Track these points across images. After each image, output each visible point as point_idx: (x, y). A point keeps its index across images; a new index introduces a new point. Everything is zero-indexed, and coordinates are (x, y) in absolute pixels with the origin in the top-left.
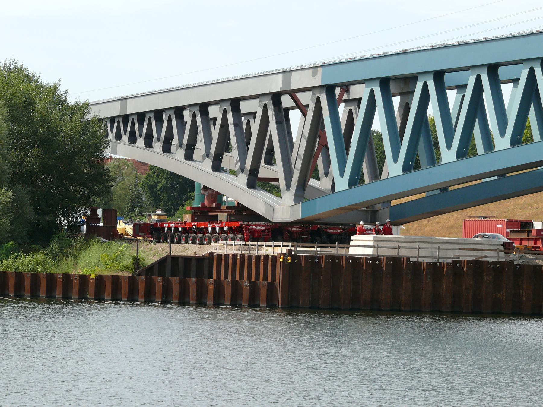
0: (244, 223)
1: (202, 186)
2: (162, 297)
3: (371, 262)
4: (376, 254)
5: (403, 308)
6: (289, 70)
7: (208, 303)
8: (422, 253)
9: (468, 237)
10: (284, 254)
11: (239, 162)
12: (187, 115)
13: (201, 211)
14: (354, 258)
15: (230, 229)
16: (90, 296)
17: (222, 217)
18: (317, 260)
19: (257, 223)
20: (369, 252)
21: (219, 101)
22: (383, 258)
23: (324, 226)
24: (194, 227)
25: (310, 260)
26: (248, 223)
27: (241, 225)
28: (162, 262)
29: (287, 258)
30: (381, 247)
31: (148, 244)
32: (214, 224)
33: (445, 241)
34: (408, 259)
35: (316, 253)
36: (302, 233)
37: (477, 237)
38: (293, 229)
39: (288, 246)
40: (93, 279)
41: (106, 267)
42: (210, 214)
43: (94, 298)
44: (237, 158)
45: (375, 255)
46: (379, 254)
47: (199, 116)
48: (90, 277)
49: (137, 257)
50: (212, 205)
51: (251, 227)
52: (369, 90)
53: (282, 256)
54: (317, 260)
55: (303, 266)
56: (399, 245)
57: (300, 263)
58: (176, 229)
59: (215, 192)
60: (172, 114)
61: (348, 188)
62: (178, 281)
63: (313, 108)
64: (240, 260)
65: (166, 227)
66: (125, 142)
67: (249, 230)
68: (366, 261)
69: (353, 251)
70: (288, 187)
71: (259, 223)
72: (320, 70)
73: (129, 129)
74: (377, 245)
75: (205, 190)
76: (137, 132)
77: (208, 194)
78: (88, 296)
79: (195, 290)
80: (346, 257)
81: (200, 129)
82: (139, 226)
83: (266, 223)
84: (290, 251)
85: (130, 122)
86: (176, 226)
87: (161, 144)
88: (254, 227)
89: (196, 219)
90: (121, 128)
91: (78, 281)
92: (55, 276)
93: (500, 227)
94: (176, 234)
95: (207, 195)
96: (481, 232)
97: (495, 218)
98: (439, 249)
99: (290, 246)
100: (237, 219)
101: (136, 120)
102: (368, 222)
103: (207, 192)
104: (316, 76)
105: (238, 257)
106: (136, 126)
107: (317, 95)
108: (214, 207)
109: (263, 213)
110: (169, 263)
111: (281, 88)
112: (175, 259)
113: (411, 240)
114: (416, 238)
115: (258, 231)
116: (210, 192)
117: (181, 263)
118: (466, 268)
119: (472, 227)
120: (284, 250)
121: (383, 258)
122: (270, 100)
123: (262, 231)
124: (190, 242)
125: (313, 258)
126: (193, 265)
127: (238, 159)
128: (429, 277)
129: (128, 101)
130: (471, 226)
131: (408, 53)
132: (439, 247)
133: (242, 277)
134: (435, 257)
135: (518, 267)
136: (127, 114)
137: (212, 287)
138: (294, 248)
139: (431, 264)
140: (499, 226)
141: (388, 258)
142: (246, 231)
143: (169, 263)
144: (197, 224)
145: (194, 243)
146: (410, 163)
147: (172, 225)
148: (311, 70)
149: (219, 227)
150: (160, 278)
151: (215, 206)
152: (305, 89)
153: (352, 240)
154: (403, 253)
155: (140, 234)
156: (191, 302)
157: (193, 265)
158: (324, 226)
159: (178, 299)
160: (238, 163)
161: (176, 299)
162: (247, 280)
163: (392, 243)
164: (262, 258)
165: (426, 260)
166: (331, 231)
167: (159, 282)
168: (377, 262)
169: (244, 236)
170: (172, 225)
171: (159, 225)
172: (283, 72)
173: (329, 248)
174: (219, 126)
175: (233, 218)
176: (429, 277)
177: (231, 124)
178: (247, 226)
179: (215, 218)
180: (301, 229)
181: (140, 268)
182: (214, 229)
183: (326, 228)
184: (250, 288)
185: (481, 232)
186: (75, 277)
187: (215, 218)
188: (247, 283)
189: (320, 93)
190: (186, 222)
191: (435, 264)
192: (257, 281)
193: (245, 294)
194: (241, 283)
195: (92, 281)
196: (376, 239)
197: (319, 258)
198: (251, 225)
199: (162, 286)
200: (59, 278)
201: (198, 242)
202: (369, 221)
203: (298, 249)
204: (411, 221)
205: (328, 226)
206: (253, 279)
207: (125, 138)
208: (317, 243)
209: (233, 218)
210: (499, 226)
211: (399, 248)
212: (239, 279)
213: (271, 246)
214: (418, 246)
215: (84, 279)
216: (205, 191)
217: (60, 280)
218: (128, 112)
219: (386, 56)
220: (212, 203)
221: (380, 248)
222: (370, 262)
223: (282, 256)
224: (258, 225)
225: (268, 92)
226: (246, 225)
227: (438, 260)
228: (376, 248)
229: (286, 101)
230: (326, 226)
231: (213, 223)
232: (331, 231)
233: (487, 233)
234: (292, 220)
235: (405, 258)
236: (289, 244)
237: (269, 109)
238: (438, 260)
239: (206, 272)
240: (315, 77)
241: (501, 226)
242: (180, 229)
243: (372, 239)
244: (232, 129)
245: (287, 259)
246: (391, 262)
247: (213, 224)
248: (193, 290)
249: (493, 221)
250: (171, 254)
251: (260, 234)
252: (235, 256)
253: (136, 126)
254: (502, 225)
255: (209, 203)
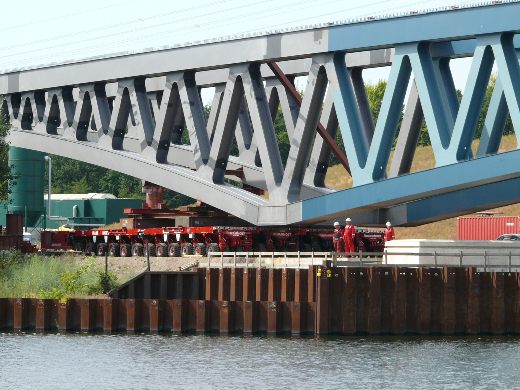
0: (219, 228)
1: (143, 183)
2: (159, 325)
3: (429, 274)
4: (434, 264)
5: (469, 331)
6: (278, 32)
7: (221, 331)
8: (494, 261)
9: (469, 238)
10: (322, 267)
11: (200, 151)
12: (76, 93)
13: (143, 215)
14: (389, 268)
15: (198, 237)
16: (60, 326)
17: (182, 221)
18: (361, 273)
19: (235, 228)
20: (414, 261)
21: (164, 73)
22: (444, 269)
23: (315, 230)
24: (140, 234)
25: (354, 274)
26: (224, 228)
27: (216, 231)
28: (139, 280)
29: (326, 272)
30: (440, 255)
31: (84, 258)
32: (173, 230)
33: (503, 245)
34: (474, 269)
35: (361, 264)
36: (289, 239)
37: (502, 238)
38: (278, 234)
39: (323, 256)
40: (64, 304)
41: (68, 288)
42: (156, 218)
43: (203, 330)
44: (196, 146)
45: (433, 265)
46: (438, 264)
47: (134, 93)
48: (60, 302)
49: (107, 275)
50: (157, 207)
51: (228, 233)
52: (401, 57)
53: (320, 270)
54: (361, 273)
55: (346, 281)
56: (461, 252)
57: (341, 276)
58: (112, 238)
59: (160, 190)
60: (91, 91)
61: (372, 181)
62: (180, 304)
63: (314, 80)
64: (249, 276)
65: (95, 235)
66: (16, 128)
67: (225, 236)
68: (399, 273)
69: (392, 261)
70: (279, 179)
71: (238, 228)
72: (326, 33)
73: (21, 111)
74: (435, 252)
75: (148, 187)
76: (35, 114)
77: (151, 192)
78: (58, 326)
79: (203, 315)
80: (423, 269)
81: (136, 109)
82: (50, 235)
83: (246, 228)
84: (328, 263)
85: (23, 103)
86: (111, 234)
87: (74, 130)
88: (231, 233)
89: (139, 224)
90: (9, 110)
91: (43, 308)
92: (11, 301)
93: (511, 226)
94: (101, 244)
95: (150, 193)
96: (506, 232)
97: (502, 215)
98: (510, 255)
99: (326, 256)
100: (202, 223)
101: (32, 99)
102: (376, 224)
103: (151, 190)
104: (320, 40)
105: (245, 272)
106: (34, 107)
107: (321, 65)
108: (161, 208)
109: (242, 215)
110: (148, 281)
111: (264, 56)
112: (156, 277)
113: (464, 245)
114: (469, 243)
115: (236, 238)
116: (155, 190)
117: (163, 282)
118: (396, 277)
119: (470, 226)
120: (319, 262)
121: (444, 269)
122: (246, 72)
123: (242, 238)
124: (135, 254)
125: (358, 270)
126: (179, 283)
127: (198, 147)
128: (500, 291)
129: (21, 75)
130: (469, 226)
131: (463, 10)
132: (510, 252)
133: (264, 296)
134: (506, 266)
135: (510, 274)
136: (20, 91)
137: (226, 311)
138: (334, 259)
139: (503, 274)
140: (509, 224)
141: (451, 269)
142: (222, 238)
143: (148, 281)
144: (146, 231)
145: (165, 254)
146: (465, 148)
147: (105, 233)
148: (312, 33)
149: (180, 234)
150: (155, 301)
151: (161, 208)
152: (303, 56)
153: (387, 247)
154: (468, 261)
155: (53, 245)
156: (198, 330)
157: (179, 283)
158: (315, 230)
159: (111, 326)
160: (198, 151)
161: (177, 326)
162: (274, 300)
163: (442, 249)
164: (233, 272)
165: (499, 270)
166: (324, 235)
167: (154, 305)
168: (436, 274)
169: (219, 245)
170: (105, 233)
171: (83, 234)
172: (268, 36)
173: (369, 257)
174: (167, 106)
175: (197, 222)
176: (500, 291)
177: (185, 103)
178: (223, 232)
179: (171, 223)
180: (288, 235)
181: (111, 289)
182: (172, 237)
183: (317, 233)
184: (277, 311)
185: (506, 232)
186: (39, 303)
187: (171, 223)
188: (273, 305)
189: (326, 62)
190: (125, 229)
191: (506, 274)
192: (214, 301)
193: (271, 319)
194: (264, 305)
195: (62, 307)
196: (423, 245)
197: (364, 270)
198: (227, 230)
199: (275, 314)
200: (271, 308)
201: (123, 254)
202: (378, 222)
203: (338, 259)
204: (432, 221)
205: (319, 230)
206: (233, 298)
207: (16, 123)
208: (360, 251)
209: (197, 222)
210: (509, 224)
211: (461, 255)
212: (287, 300)
213: (270, 256)
214: (486, 252)
215: (28, 303)
216: (148, 188)
217: (19, 306)
218: (21, 90)
219: (428, 14)
220: (157, 204)
221: (439, 256)
222: (353, 273)
223: (320, 270)
224: (236, 231)
225: (245, 61)
226: (223, 230)
227: (510, 270)
228: (434, 256)
229: (265, 71)
230: (317, 230)
231: (171, 229)
232: (324, 235)
233: (517, 233)
234: (289, 223)
235: (470, 268)
236: (325, 253)
237: (245, 83)
238: (510, 270)
239: (195, 291)
240: (318, 42)
241: (512, 224)
242: (118, 238)
243: (418, 245)
244: (187, 110)
245: (326, 273)
246: (454, 273)
247: (170, 231)
248: (177, 316)
249: (472, 220)
250: (149, 270)
251: (240, 242)
252: (227, 271)
253: (34, 107)
254: (514, 222)
255: (153, 204)
